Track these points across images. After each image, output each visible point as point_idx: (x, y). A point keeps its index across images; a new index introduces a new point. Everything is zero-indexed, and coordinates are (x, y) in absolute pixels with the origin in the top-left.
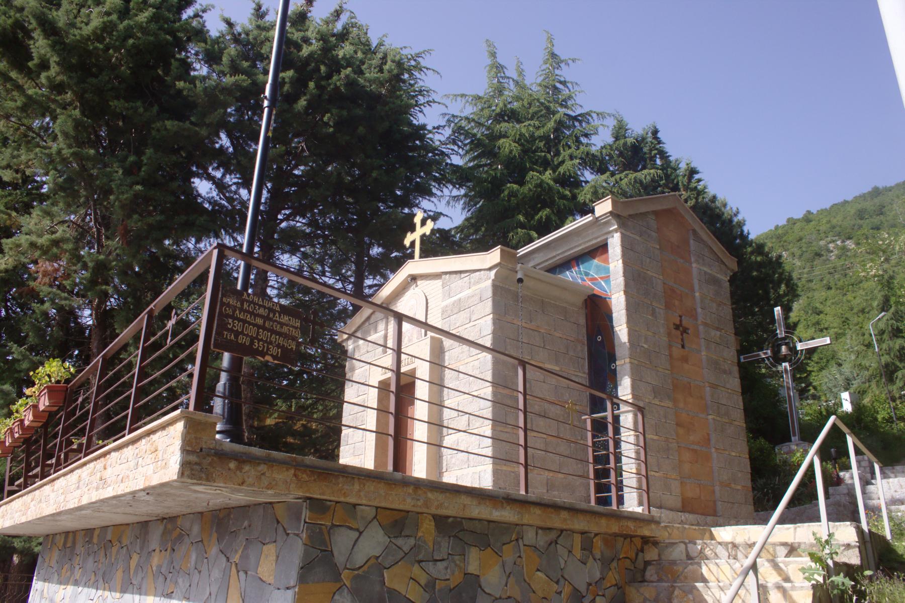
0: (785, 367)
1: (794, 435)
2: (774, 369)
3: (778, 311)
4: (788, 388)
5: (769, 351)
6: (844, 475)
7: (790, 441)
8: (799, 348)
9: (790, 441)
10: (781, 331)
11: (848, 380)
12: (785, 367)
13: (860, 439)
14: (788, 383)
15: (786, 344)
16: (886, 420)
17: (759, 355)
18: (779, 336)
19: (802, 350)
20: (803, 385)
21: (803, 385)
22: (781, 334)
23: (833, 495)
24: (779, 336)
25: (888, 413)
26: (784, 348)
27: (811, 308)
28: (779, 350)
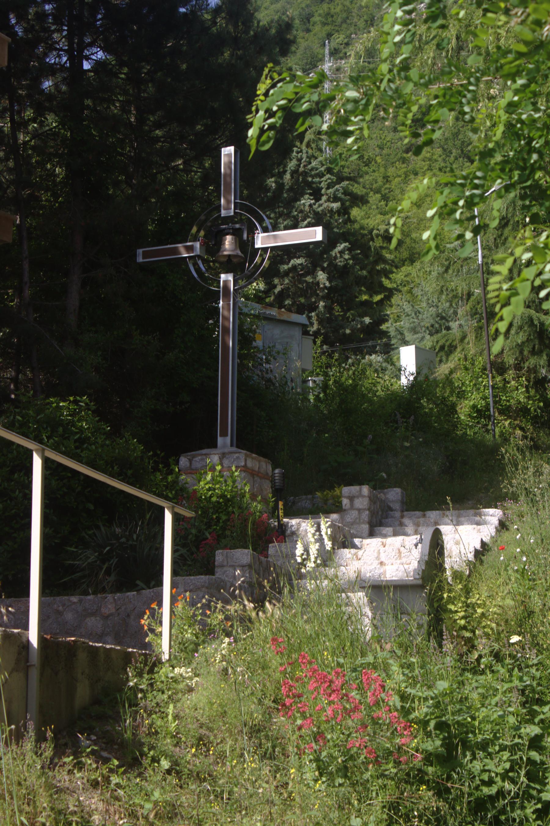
0: (226, 282)
1: (224, 434)
2: (309, 279)
3: (229, 155)
4: (226, 330)
5: (197, 245)
6: (299, 525)
7: (214, 445)
8: (258, 245)
9: (214, 445)
10: (228, 202)
11: (442, 318)
12: (226, 282)
13: (56, 448)
14: (226, 319)
15: (237, 233)
16: (478, 411)
17: (176, 251)
18: (223, 213)
19: (265, 250)
20: (367, 320)
21: (367, 320)
22: (228, 208)
23: (222, 566)
24: (223, 213)
25: (485, 398)
26: (228, 240)
27: (458, 143)
28: (220, 243)
